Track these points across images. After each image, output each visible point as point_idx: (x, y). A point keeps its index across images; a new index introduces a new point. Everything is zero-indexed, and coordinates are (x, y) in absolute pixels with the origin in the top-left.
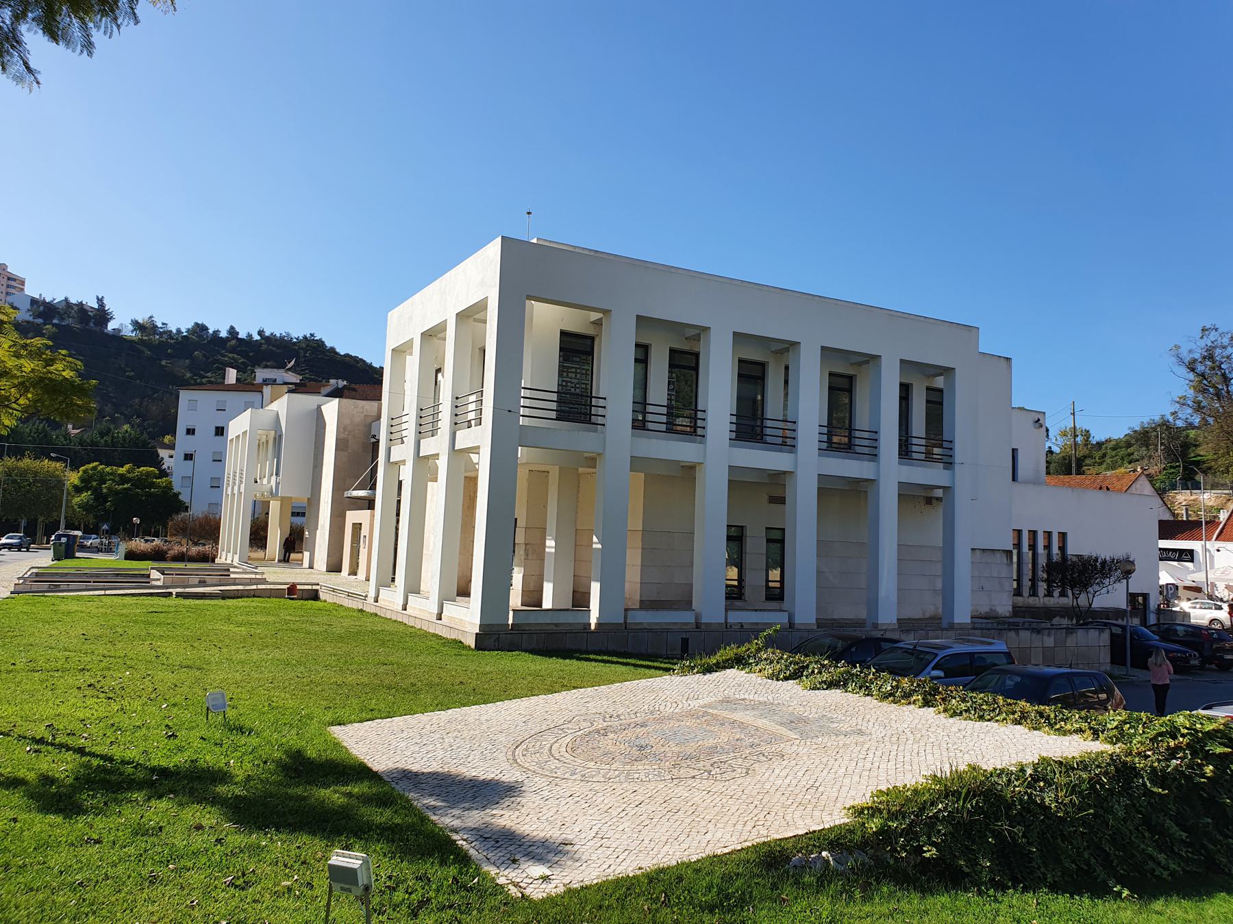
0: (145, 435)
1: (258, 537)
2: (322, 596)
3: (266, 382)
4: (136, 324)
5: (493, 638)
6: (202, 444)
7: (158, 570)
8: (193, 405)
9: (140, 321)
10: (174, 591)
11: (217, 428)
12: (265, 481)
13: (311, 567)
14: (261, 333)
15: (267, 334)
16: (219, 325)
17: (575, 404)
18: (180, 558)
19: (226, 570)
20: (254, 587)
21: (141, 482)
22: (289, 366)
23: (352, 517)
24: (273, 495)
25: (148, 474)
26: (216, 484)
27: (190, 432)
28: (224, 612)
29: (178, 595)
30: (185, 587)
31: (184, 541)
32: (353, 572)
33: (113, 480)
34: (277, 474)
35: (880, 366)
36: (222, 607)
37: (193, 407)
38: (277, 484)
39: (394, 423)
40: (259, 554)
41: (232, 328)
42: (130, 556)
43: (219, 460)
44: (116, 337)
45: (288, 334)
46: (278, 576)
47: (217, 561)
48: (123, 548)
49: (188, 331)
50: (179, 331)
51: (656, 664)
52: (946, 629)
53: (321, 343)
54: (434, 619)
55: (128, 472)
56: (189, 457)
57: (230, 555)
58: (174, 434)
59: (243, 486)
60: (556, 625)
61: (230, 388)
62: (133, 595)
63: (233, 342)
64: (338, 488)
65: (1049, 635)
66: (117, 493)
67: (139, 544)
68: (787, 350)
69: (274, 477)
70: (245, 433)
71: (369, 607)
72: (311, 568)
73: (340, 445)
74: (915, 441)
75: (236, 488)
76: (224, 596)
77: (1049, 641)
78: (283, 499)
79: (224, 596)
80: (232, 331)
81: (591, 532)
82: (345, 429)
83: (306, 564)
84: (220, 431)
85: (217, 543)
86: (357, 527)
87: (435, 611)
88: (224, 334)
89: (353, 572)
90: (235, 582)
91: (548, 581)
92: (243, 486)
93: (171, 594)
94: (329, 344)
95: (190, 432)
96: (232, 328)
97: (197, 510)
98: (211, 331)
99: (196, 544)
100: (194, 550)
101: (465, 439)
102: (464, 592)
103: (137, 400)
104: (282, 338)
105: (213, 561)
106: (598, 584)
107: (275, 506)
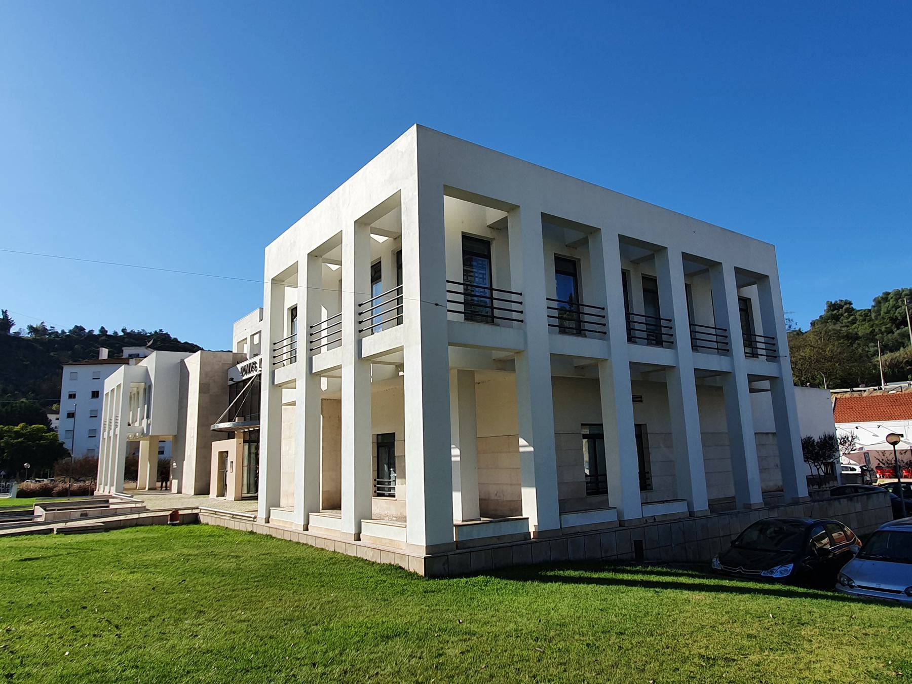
0: (37, 405)
1: (131, 472)
2: (203, 519)
3: (131, 356)
4: (31, 328)
5: (449, 560)
6: (83, 403)
7: (44, 507)
9: (35, 326)
10: (55, 526)
11: (97, 396)
12: (137, 424)
13: (179, 492)
14: (124, 330)
15: (128, 331)
16: (93, 326)
17: (480, 304)
18: (64, 493)
19: (106, 501)
20: (136, 516)
21: (34, 437)
22: (149, 344)
23: (218, 447)
24: (144, 435)
25: (39, 430)
26: (94, 434)
27: (72, 396)
28: (110, 550)
29: (60, 531)
30: (66, 522)
31: (67, 480)
32: (222, 492)
33: (10, 436)
34: (148, 417)
35: (721, 273)
36: (107, 543)
37: (74, 378)
38: (148, 425)
39: (276, 347)
40: (131, 485)
41: (103, 328)
42: (22, 494)
43: (95, 415)
44: (17, 337)
46: (159, 503)
47: (96, 493)
48: (16, 487)
49: (70, 331)
50: (63, 332)
51: (620, 576)
52: (790, 505)
53: (167, 335)
54: (351, 540)
55: (22, 429)
56: (71, 415)
57: (107, 488)
58: (59, 402)
59: (118, 430)
60: (499, 538)
61: (104, 362)
62: (13, 535)
63: (104, 338)
64: (203, 422)
65: (857, 501)
66: (13, 445)
67: (30, 484)
68: (651, 258)
69: (145, 420)
70: (119, 386)
71: (260, 528)
72: (182, 495)
74: (758, 339)
75: (112, 432)
76: (107, 528)
77: (858, 507)
78: (152, 439)
79: (107, 528)
80: (103, 330)
81: (516, 437)
82: (206, 375)
83: (174, 488)
84: (95, 394)
86: (223, 455)
87: (352, 530)
88: (96, 332)
89: (222, 492)
90: (115, 513)
91: (458, 491)
92: (118, 430)
93: (51, 530)
94: (173, 336)
95: (72, 396)
96: (103, 328)
97: (78, 454)
98: (87, 331)
99: (77, 481)
100: (76, 486)
102: (334, 504)
103: (32, 381)
104: (139, 333)
105: (92, 494)
106: (533, 491)
107: (144, 446)
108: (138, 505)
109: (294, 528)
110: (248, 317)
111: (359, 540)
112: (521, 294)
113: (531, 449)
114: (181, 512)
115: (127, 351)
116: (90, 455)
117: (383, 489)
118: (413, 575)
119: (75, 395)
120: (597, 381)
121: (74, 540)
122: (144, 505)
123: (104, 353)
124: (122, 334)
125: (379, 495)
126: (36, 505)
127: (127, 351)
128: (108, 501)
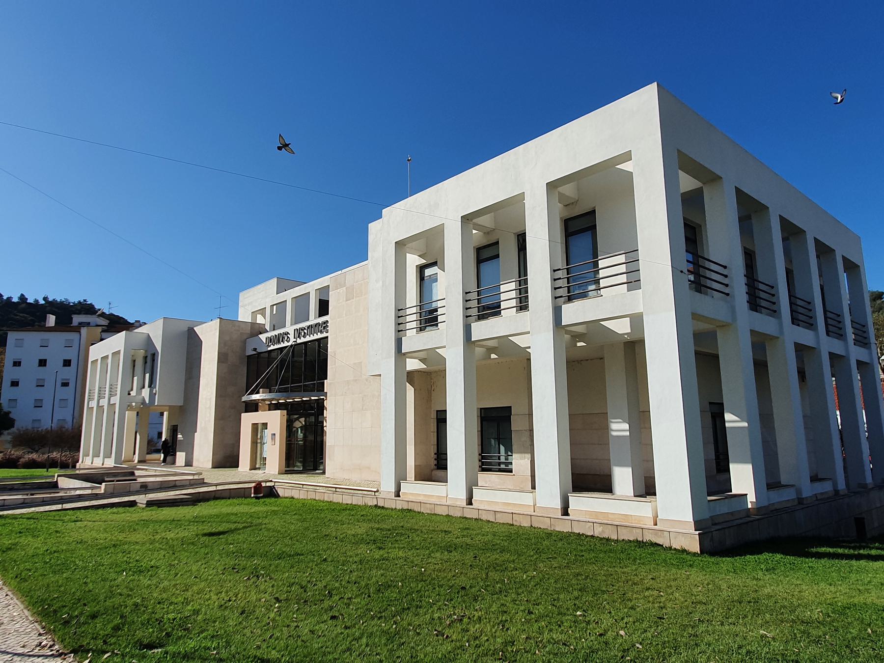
2: (281, 492)
3: (81, 325)
5: (727, 534)
8: (19, 343)
14: (45, 299)
15: (50, 299)
23: (248, 419)
27: (17, 364)
38: (152, 396)
41: (22, 295)
45: (67, 300)
60: (732, 514)
61: (50, 329)
63: (24, 305)
73: (222, 358)
85: (78, 449)
93: (133, 504)
95: (17, 364)
96: (22, 295)
98: (5, 298)
101: (607, 306)
104: (62, 303)
105: (74, 467)
108: (196, 477)
109: (459, 503)
110: (263, 285)
111: (567, 514)
112: (725, 267)
113: (746, 424)
114: (264, 484)
115: (77, 319)
116: (36, 425)
117: (490, 464)
118: (695, 554)
119: (20, 362)
120: (716, 357)
121: (253, 511)
122: (201, 477)
123: (51, 320)
124: (43, 302)
125: (483, 470)
126: (58, 476)
127: (77, 319)
128: (133, 474)
